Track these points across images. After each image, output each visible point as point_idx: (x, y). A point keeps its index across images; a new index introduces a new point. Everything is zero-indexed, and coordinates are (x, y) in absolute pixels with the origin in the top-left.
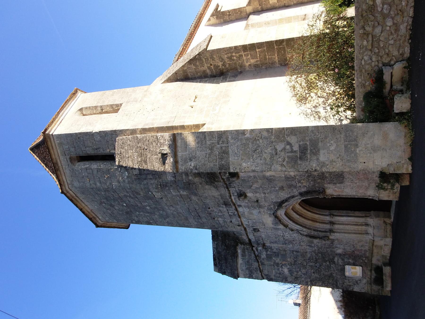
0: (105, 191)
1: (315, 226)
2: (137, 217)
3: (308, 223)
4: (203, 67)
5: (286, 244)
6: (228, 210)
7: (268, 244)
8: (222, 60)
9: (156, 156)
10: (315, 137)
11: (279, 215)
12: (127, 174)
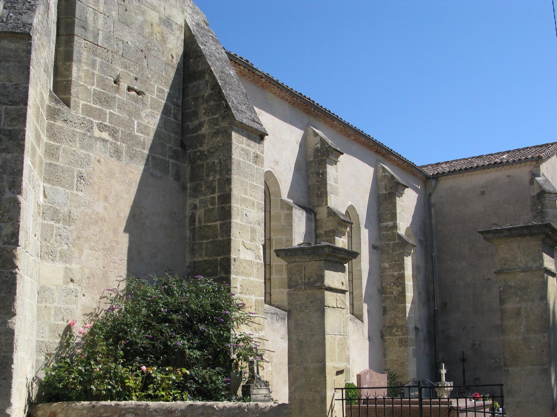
4: (205, 114)
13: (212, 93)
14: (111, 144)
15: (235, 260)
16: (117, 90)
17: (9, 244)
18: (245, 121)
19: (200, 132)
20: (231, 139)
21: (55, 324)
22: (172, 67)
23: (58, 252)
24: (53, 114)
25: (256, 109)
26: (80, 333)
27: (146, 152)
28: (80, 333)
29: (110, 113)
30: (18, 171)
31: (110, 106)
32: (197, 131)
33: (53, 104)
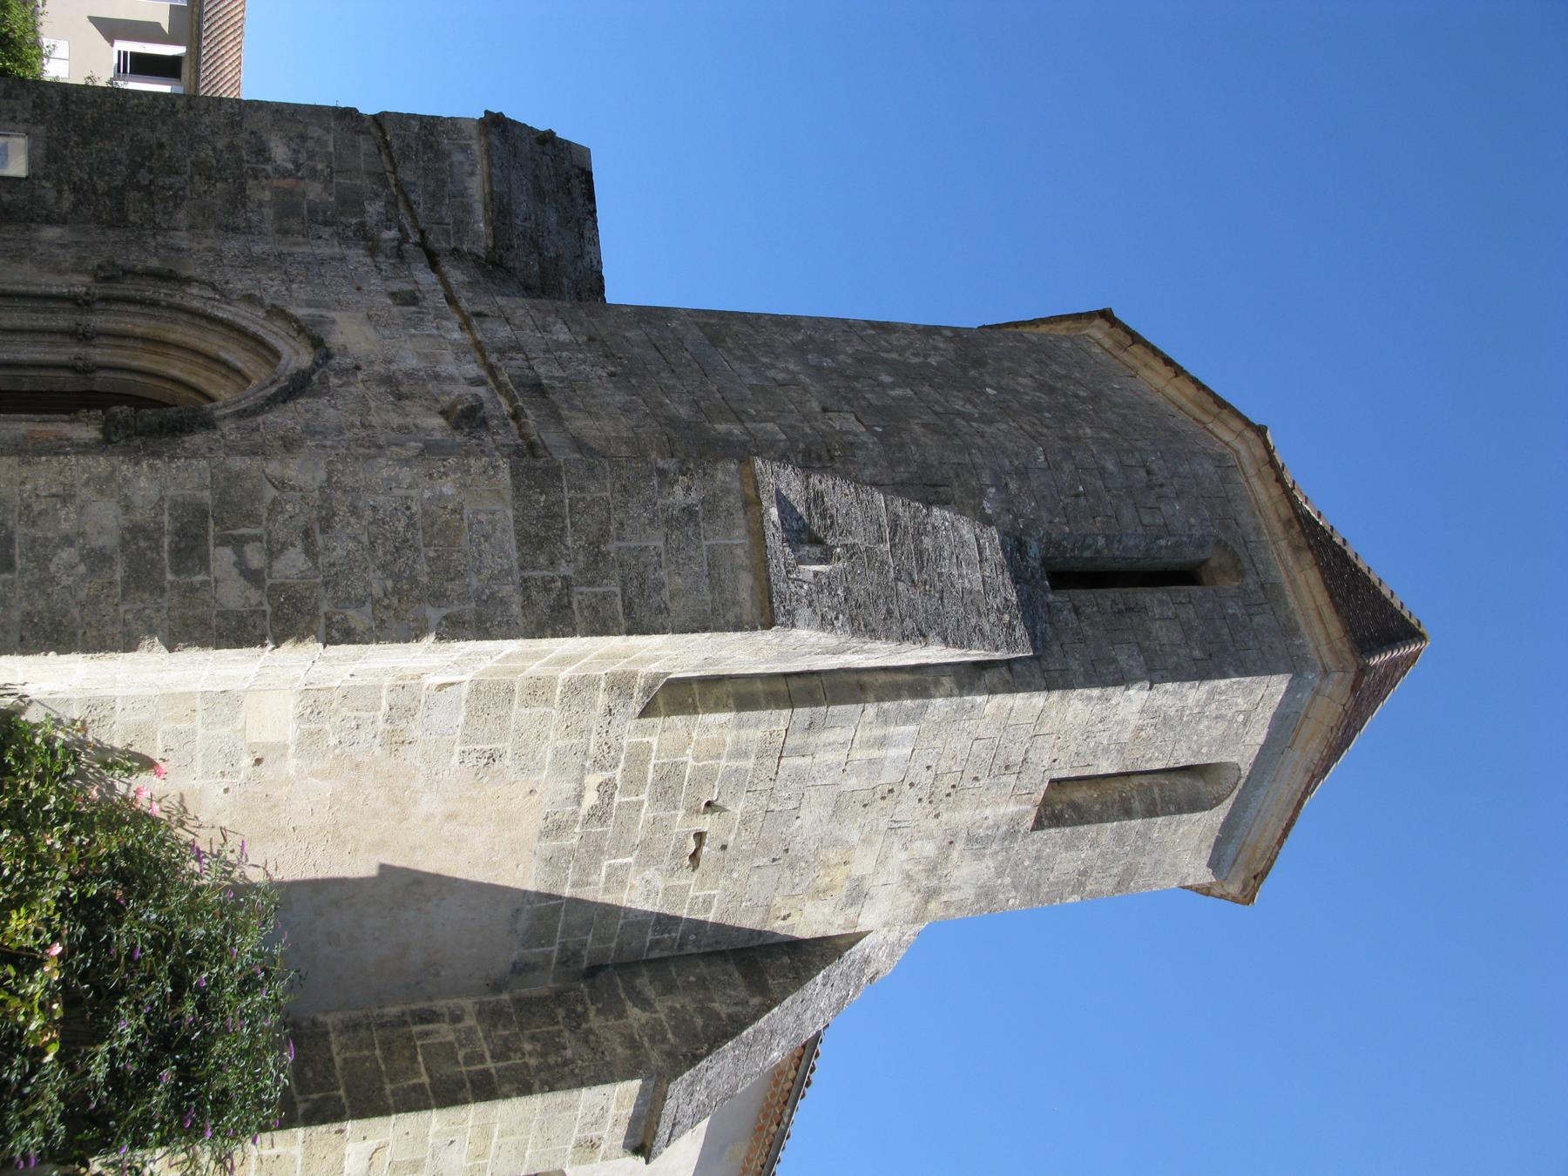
0: (1079, 439)
1: (153, 322)
2: (935, 348)
3: (179, 332)
4: (672, 1009)
5: (280, 256)
6: (531, 368)
7: (357, 255)
8: (586, 1038)
9: (850, 540)
10: (139, 605)
11: (302, 351)
12: (986, 504)
13: (720, 1019)
14: (574, 813)
15: (341, 1131)
16: (693, 811)
17: (327, 626)
18: (670, 1104)
19: (629, 1004)
20: (623, 1080)
21: (155, 733)
22: (764, 921)
23: (319, 726)
24: (620, 685)
25: (704, 1124)
26: (137, 792)
27: (567, 892)
28: (137, 792)
29: (641, 803)
30: (487, 630)
31: (656, 799)
32: (630, 998)
33: (641, 682)
